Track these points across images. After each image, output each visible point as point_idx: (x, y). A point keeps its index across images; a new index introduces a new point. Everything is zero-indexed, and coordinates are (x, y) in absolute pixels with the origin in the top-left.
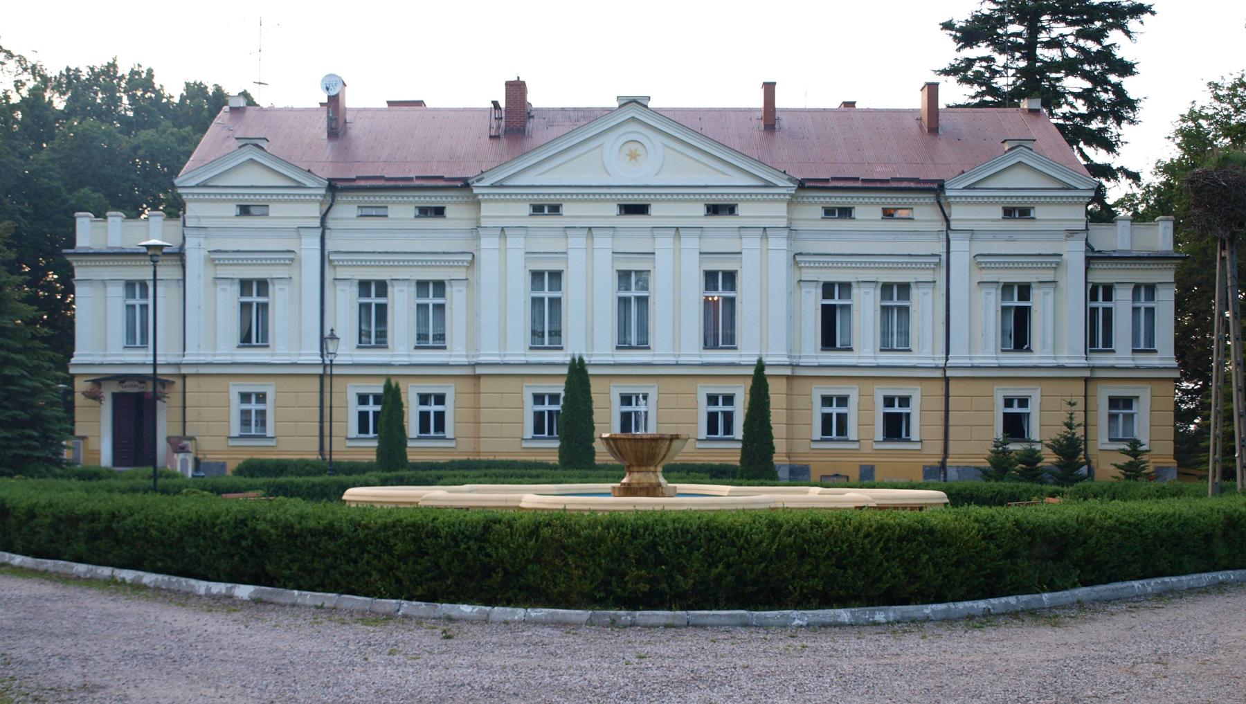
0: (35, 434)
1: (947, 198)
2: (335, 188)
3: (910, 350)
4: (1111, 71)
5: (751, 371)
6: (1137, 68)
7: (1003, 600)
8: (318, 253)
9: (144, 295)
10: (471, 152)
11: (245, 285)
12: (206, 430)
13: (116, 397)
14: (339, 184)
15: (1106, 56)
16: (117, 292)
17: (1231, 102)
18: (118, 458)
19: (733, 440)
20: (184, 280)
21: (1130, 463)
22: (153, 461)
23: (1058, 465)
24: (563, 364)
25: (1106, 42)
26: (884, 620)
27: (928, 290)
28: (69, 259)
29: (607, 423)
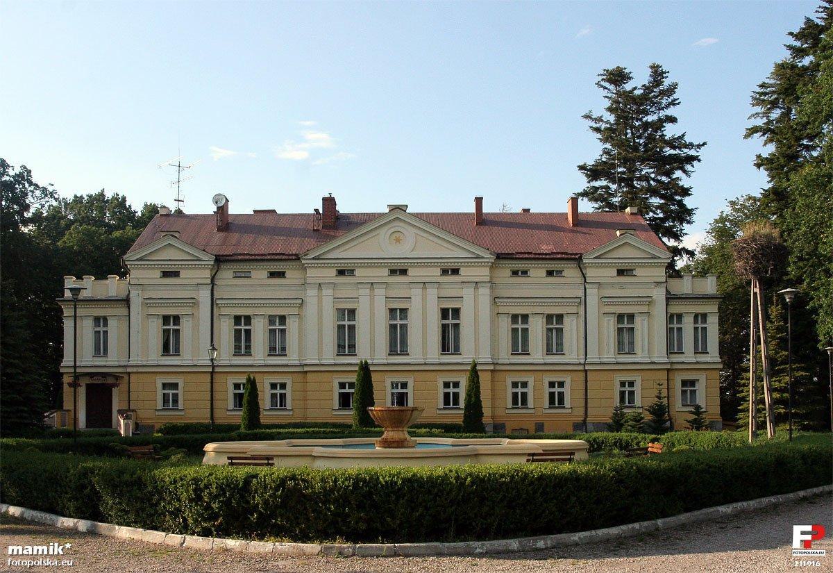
0: (26, 409)
2: (220, 260)
3: (564, 354)
4: (676, 194)
5: (469, 368)
6: (692, 191)
7: (630, 526)
8: (209, 299)
11: (166, 319)
13: (87, 385)
14: (222, 258)
17: (743, 212)
18: (89, 422)
19: (459, 408)
20: (129, 316)
21: (695, 419)
23: (654, 421)
24: (357, 364)
25: (674, 176)
26: (543, 547)
27: (574, 318)
29: (383, 400)
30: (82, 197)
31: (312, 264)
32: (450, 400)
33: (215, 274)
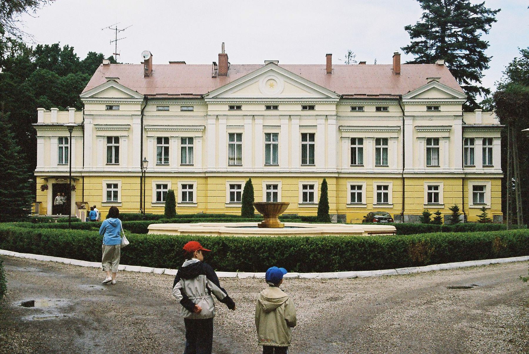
1: (403, 102)
2: (147, 99)
3: (388, 166)
8: (140, 125)
9: (67, 142)
10: (204, 84)
12: (93, 197)
13: (54, 185)
15: (475, 39)
16: (56, 141)
22: (69, 213)
25: (476, 34)
28: (35, 127)
30: (42, 46)
31: (211, 101)
32: (308, 197)
33: (144, 108)
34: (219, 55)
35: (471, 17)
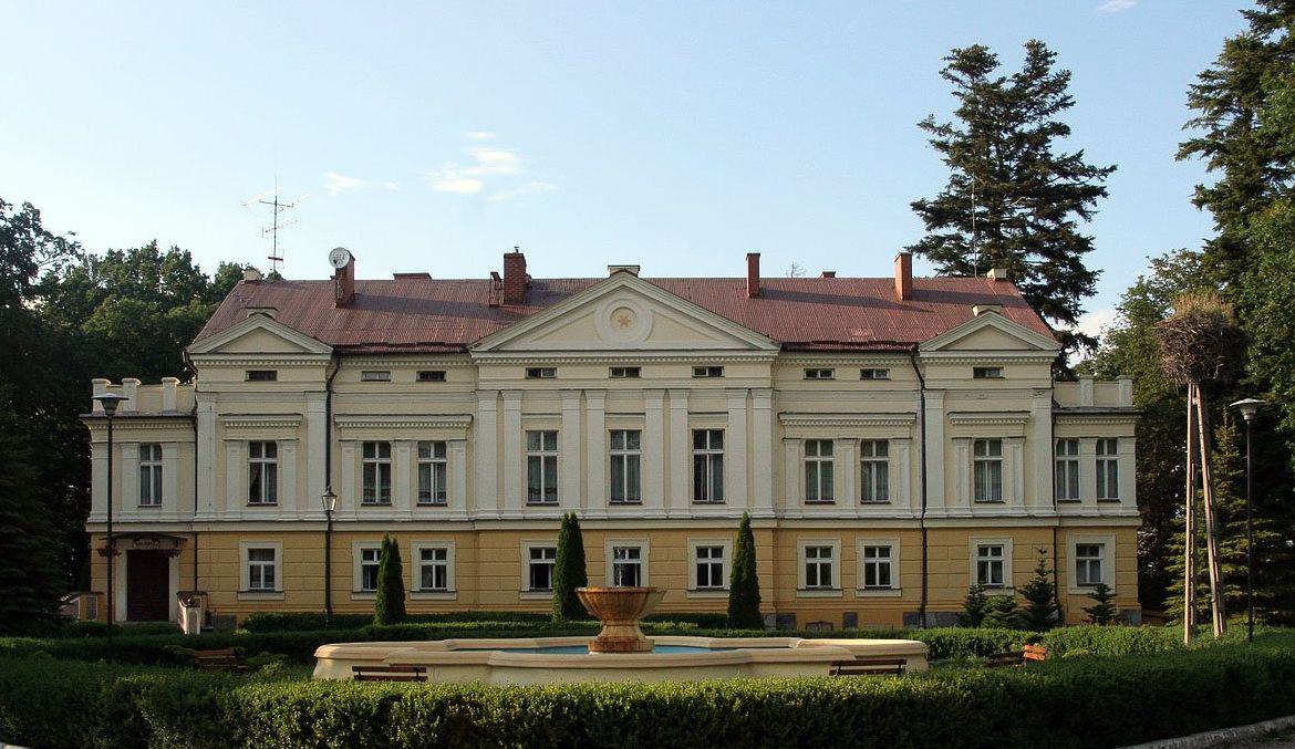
2: (340, 354)
25: (1065, 220)
33: (333, 376)
34: (505, 256)
35: (1053, 185)
